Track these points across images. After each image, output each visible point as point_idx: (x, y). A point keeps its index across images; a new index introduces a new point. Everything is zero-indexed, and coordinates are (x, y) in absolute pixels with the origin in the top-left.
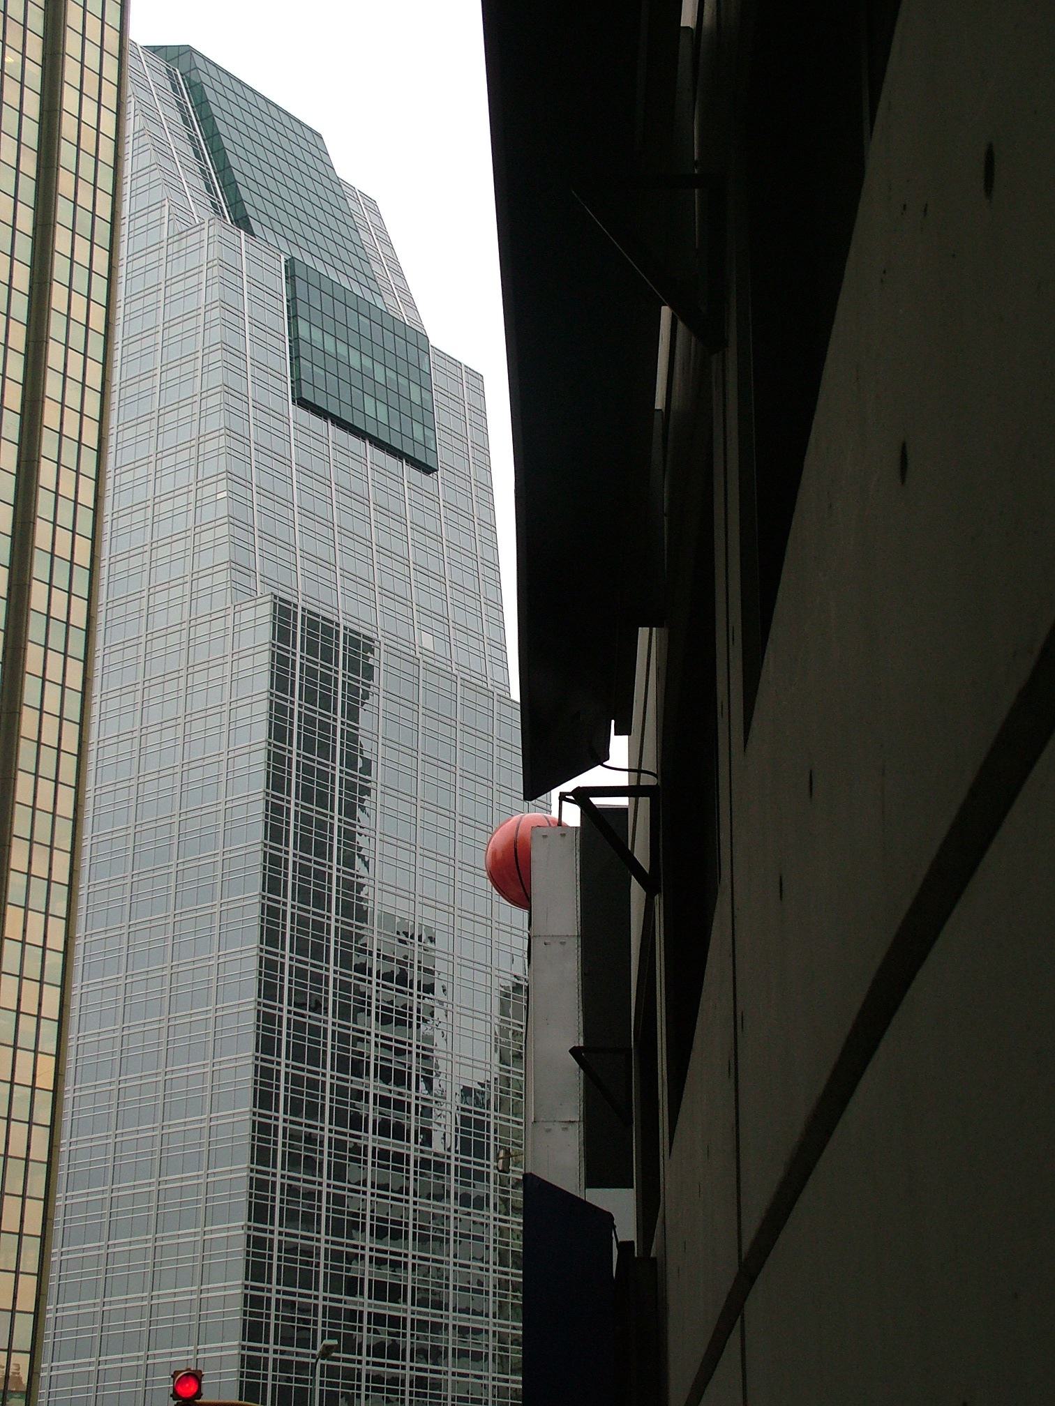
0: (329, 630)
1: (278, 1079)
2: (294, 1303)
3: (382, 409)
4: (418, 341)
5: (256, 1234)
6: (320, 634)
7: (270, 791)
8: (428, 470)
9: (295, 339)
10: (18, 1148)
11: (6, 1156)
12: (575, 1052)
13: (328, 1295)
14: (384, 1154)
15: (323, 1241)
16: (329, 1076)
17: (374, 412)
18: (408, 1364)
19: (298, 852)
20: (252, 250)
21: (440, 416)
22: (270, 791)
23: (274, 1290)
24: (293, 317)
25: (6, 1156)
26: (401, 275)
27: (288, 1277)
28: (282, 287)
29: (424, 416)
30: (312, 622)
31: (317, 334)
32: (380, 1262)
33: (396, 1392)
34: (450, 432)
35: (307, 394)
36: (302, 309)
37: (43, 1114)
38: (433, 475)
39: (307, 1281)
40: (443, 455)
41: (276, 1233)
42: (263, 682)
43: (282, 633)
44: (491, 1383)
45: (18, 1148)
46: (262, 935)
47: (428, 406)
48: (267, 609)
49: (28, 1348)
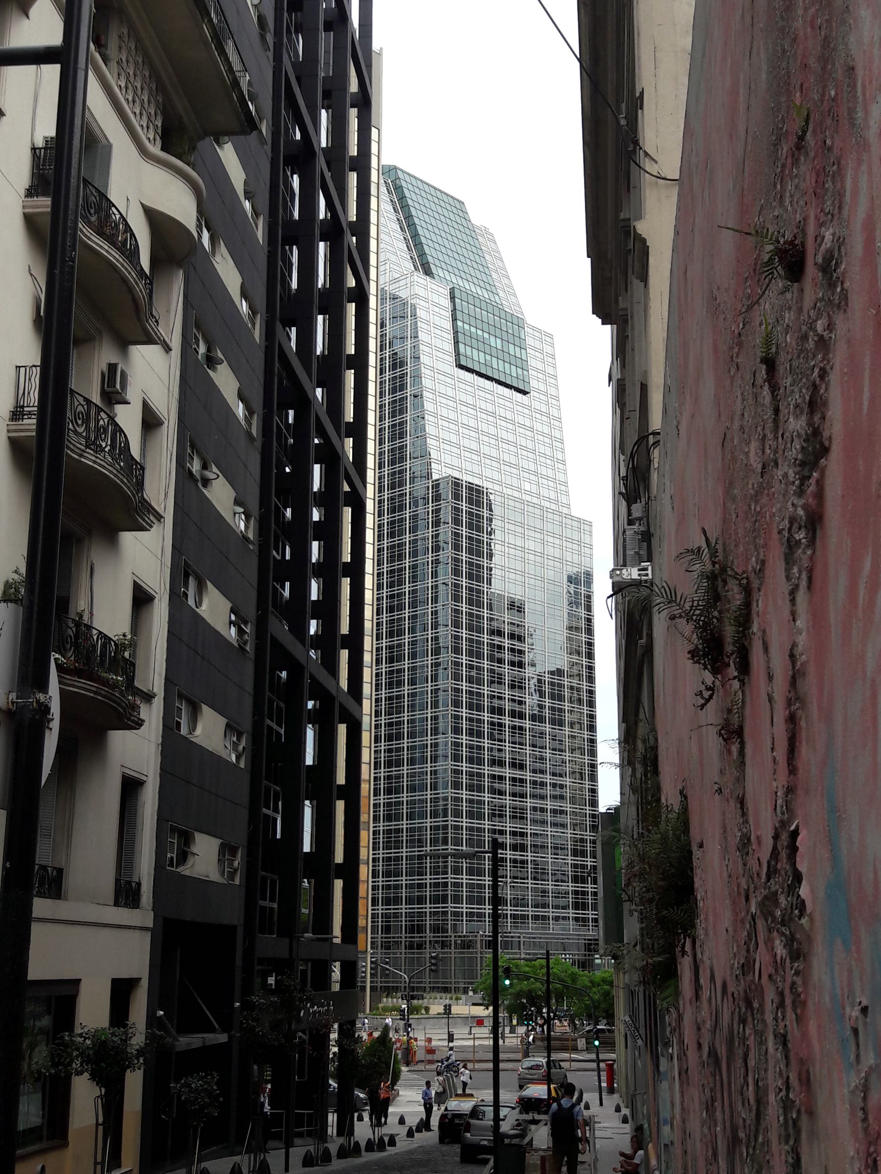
2: (473, 800)
3: (499, 341)
4: (519, 323)
8: (525, 393)
9: (456, 333)
12: (603, 323)
14: (515, 861)
16: (486, 638)
17: (498, 367)
18: (528, 800)
20: (434, 286)
21: (532, 362)
24: (454, 319)
26: (508, 277)
27: (471, 760)
28: (446, 303)
29: (522, 365)
30: (471, 488)
31: (467, 327)
32: (513, 701)
33: (524, 868)
34: (537, 370)
35: (463, 363)
36: (459, 315)
38: (528, 395)
40: (534, 383)
44: (570, 862)
47: (524, 358)
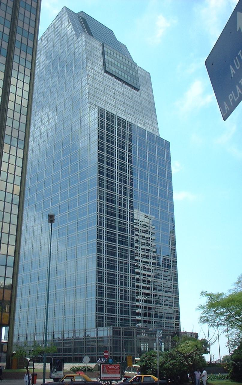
0: (113, 116)
1: (103, 260)
5: (99, 315)
6: (111, 117)
7: (99, 117)
8: (138, 90)
10: (6, 230)
11: (2, 232)
13: (120, 315)
15: (117, 301)
19: (107, 154)
22: (98, 268)
23: (104, 299)
25: (2, 232)
35: (107, 70)
37: (22, 137)
39: (113, 296)
40: (141, 88)
41: (104, 314)
42: (96, 137)
43: (101, 115)
45: (6, 230)
46: (97, 265)
48: (97, 110)
49: (13, 266)
